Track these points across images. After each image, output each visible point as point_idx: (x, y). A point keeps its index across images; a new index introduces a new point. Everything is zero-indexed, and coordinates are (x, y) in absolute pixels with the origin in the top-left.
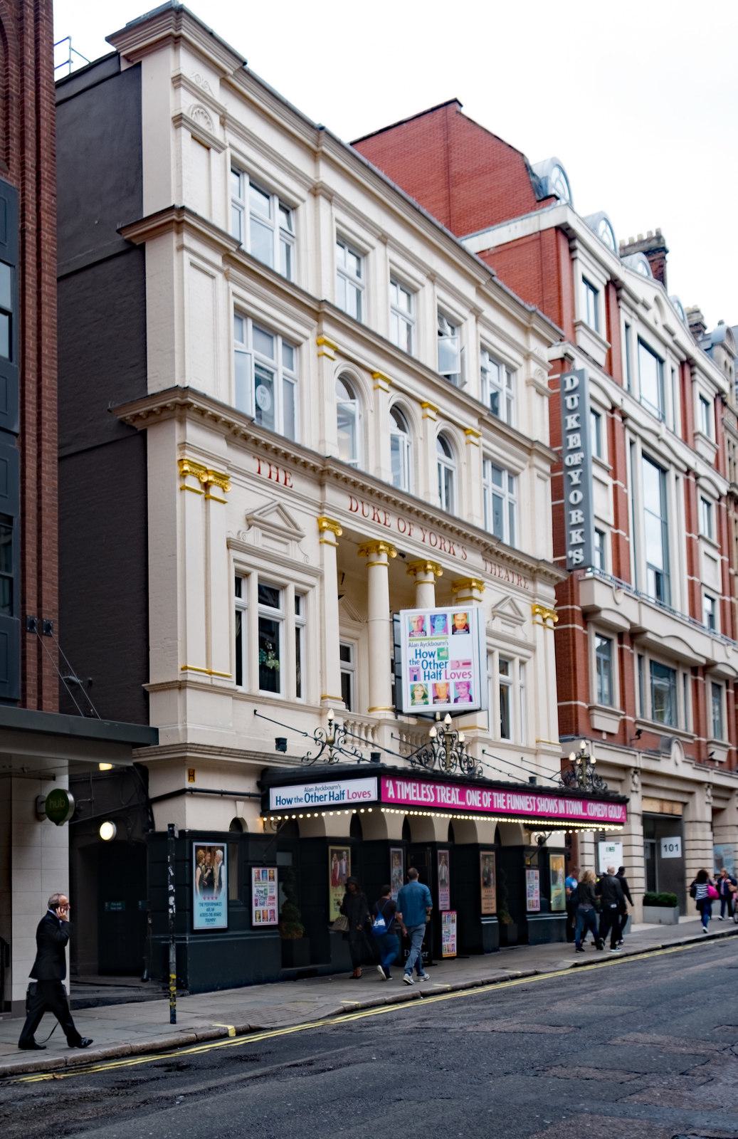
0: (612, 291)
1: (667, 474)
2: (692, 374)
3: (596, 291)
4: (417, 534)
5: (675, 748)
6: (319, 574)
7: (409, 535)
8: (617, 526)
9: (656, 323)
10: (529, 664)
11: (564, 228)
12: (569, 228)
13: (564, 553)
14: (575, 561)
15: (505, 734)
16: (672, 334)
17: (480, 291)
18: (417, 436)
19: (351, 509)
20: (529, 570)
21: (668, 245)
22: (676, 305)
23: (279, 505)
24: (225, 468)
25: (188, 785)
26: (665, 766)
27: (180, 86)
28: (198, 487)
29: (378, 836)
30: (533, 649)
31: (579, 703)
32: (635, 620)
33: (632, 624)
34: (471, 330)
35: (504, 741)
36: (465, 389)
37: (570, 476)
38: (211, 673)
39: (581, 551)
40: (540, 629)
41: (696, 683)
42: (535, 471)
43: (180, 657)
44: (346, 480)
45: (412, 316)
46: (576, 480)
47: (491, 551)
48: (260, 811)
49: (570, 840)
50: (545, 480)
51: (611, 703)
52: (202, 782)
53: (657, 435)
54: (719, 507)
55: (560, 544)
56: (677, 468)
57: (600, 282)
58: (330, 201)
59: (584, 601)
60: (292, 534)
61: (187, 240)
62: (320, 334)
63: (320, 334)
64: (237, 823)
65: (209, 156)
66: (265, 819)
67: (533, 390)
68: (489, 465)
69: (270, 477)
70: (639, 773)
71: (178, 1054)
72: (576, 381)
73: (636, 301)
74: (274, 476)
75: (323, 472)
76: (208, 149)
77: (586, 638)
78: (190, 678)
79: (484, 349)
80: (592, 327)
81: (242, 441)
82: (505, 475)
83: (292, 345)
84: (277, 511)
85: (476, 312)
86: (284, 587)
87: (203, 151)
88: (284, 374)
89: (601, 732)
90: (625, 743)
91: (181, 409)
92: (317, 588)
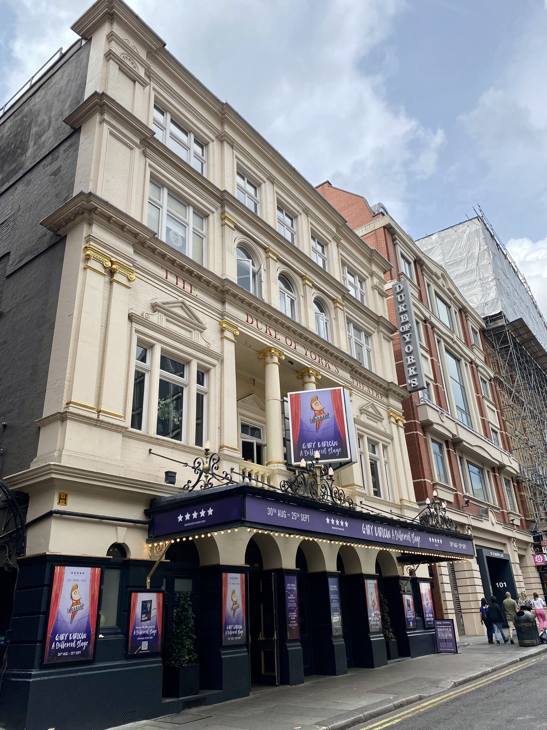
2: (466, 317)
4: (301, 350)
5: (490, 514)
7: (295, 348)
9: (444, 286)
10: (390, 448)
15: (377, 493)
16: (453, 294)
20: (386, 390)
23: (183, 303)
24: (131, 265)
25: (57, 507)
26: (485, 525)
27: (113, 39)
31: (426, 480)
33: (454, 435)
34: (333, 246)
37: (404, 337)
39: (416, 379)
40: (394, 427)
41: (495, 476)
42: (105, 126)
43: (65, 394)
44: (242, 301)
46: (408, 339)
47: (356, 372)
49: (432, 572)
50: (389, 342)
51: (447, 482)
52: (74, 505)
53: (452, 339)
54: (491, 384)
55: (400, 371)
56: (465, 359)
58: (232, 147)
59: (422, 418)
62: (223, 213)
63: (223, 213)
64: (119, 549)
65: (135, 85)
66: (150, 545)
67: (376, 292)
69: (266, 332)
71: (339, 723)
72: (411, 348)
75: (221, 291)
76: (134, 82)
79: (344, 264)
80: (409, 276)
82: (363, 334)
84: (181, 307)
86: (189, 362)
87: (131, 83)
91: (89, 214)
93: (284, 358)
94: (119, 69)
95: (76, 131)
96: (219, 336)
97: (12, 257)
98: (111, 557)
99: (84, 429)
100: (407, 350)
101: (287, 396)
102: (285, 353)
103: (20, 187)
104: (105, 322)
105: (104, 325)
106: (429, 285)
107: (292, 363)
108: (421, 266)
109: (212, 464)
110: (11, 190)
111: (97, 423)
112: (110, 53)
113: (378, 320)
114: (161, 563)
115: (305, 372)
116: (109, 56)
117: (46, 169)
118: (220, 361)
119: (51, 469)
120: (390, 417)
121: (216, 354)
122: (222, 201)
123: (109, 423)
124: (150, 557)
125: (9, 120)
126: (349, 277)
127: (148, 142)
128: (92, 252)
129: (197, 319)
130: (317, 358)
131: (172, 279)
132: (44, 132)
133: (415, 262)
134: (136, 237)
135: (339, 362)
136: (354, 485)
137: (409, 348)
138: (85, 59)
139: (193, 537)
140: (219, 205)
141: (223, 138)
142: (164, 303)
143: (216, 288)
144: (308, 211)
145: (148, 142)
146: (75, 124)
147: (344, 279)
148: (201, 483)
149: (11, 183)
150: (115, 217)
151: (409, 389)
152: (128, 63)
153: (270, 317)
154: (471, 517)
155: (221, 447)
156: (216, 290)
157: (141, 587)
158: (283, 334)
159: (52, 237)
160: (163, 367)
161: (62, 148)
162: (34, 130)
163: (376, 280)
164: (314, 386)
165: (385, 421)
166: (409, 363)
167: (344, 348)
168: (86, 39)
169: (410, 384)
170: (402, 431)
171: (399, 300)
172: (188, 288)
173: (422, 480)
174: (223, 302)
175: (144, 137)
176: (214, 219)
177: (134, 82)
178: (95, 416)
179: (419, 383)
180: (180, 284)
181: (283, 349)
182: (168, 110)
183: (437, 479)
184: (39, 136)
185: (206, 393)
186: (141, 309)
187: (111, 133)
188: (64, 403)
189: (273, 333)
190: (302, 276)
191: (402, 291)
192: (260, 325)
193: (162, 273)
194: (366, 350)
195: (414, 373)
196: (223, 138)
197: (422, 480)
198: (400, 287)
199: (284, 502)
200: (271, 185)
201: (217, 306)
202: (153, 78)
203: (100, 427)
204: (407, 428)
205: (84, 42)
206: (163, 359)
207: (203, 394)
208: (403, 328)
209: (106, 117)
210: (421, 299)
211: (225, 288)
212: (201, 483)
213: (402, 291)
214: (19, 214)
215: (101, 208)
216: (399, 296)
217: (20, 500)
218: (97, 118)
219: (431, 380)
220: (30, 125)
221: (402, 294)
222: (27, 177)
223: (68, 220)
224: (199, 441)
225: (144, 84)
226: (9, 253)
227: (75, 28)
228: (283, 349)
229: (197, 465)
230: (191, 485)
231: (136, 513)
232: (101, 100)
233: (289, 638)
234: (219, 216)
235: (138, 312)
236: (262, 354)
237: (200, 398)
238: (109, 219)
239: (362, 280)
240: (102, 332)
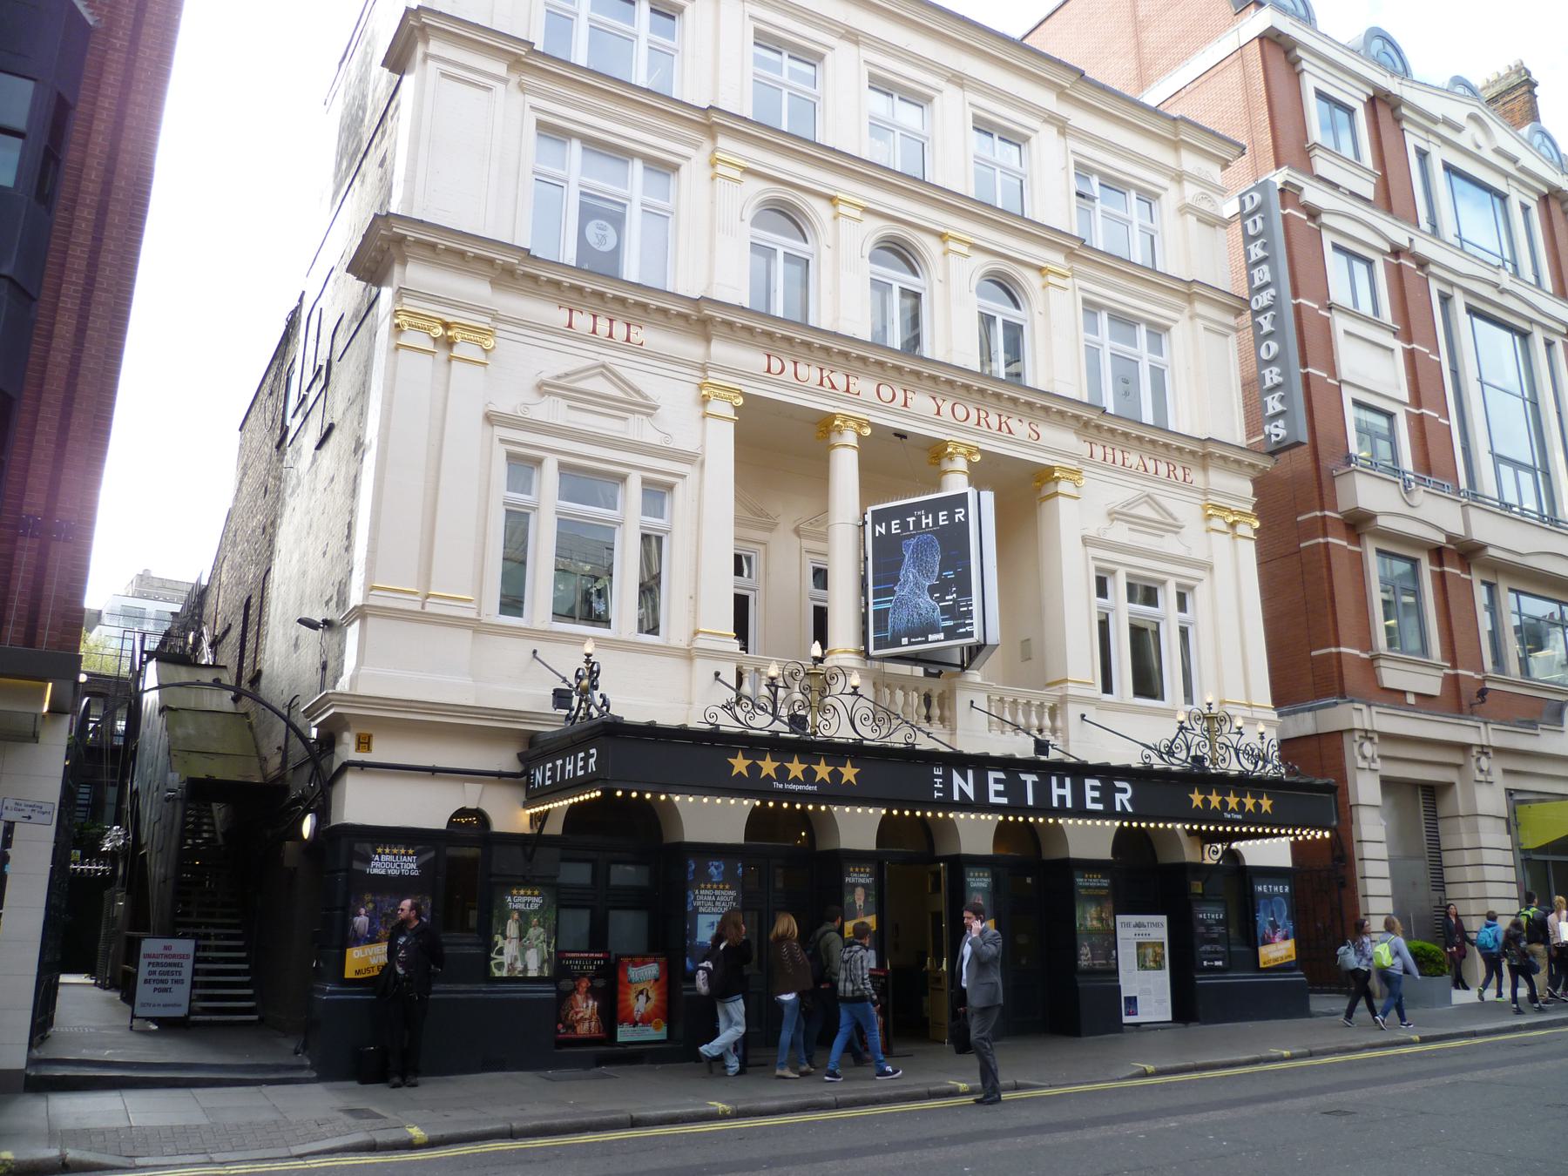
0: (1384, 114)
1: (1530, 339)
3: (1350, 111)
8: (1417, 400)
12: (1280, 34)
14: (1274, 439)
16: (1514, 160)
19: (769, 371)
21: (1535, 77)
23: (604, 366)
24: (488, 320)
28: (1224, 528)
29: (1057, 854)
30: (1208, 567)
31: (1343, 649)
32: (1458, 529)
34: (1046, 141)
35: (1107, 697)
38: (1250, 706)
39: (1281, 423)
42: (1199, 323)
45: (1022, 170)
48: (523, 798)
52: (381, 752)
53: (1496, 286)
57: (1356, 98)
59: (1344, 505)
67: (1191, 219)
68: (1103, 318)
69: (821, 384)
70: (1376, 739)
73: (1434, 120)
74: (1110, 458)
77: (1359, 561)
78: (1071, 691)
83: (663, 167)
84: (602, 374)
85: (1051, 119)
86: (1163, 583)
89: (1404, 692)
106: (1423, 155)
130: (974, 413)
131: (583, 321)
136: (1066, 680)
139: (656, 794)
142: (559, 377)
158: (871, 376)
160: (1131, 599)
164: (964, 479)
172: (620, 330)
178: (417, 607)
185: (534, 509)
186: (1096, 525)
192: (803, 370)
193: (558, 316)
197: (1333, 650)
200: (852, 48)
206: (1131, 588)
215: (412, 234)
224: (1188, 695)
231: (504, 759)
232: (418, 19)
233: (64, 978)
237: (1184, 632)
239: (1149, 197)
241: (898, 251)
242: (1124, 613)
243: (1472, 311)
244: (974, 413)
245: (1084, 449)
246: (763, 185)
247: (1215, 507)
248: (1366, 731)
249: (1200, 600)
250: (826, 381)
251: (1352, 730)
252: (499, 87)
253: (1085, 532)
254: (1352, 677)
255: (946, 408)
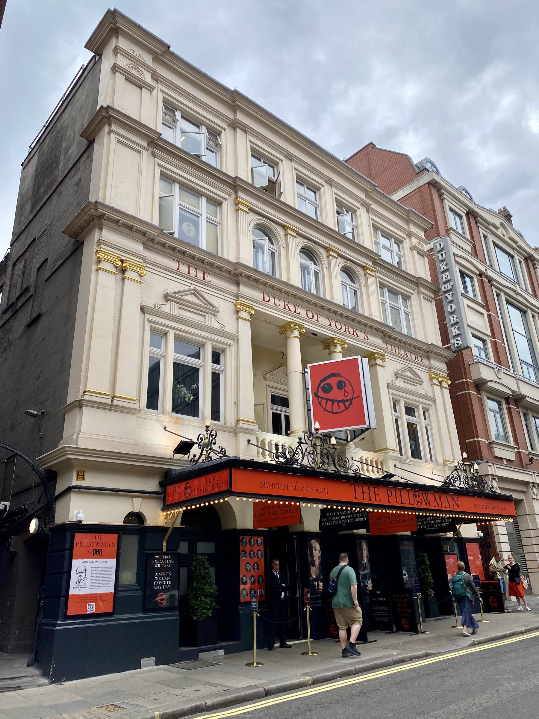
2: (534, 265)
3: (460, 217)
4: (324, 321)
6: (236, 339)
7: (317, 320)
8: (493, 336)
10: (432, 411)
11: (433, 183)
12: (436, 183)
13: (449, 342)
16: (516, 242)
17: (367, 195)
18: (324, 265)
19: (264, 300)
21: (511, 213)
22: (464, 192)
23: (195, 290)
24: (142, 261)
25: (75, 482)
28: (438, 383)
31: (480, 439)
32: (515, 389)
33: (513, 392)
34: (362, 213)
36: (282, 199)
39: (459, 339)
40: (437, 389)
46: (450, 298)
47: (390, 337)
48: (162, 506)
50: (431, 302)
51: (507, 440)
52: (90, 481)
53: (515, 291)
55: (445, 338)
56: (532, 310)
58: (245, 132)
59: (475, 376)
60: (419, 382)
61: (114, 127)
62: (237, 198)
64: (136, 517)
66: (165, 513)
67: (415, 253)
72: (454, 307)
73: (489, 223)
74: (394, 350)
75: (236, 274)
76: (141, 88)
79: (376, 228)
80: (460, 231)
81: (376, 332)
84: (194, 294)
86: (204, 345)
87: (138, 90)
88: (179, 205)
89: (502, 459)
90: (523, 467)
92: (433, 406)
93: (304, 331)
94: (125, 79)
95: (91, 143)
96: (235, 317)
97: (49, 262)
98: (127, 524)
99: (100, 414)
100: (449, 310)
101: (307, 368)
102: (305, 326)
103: (55, 198)
104: (118, 316)
105: (117, 319)
106: (485, 237)
107: (315, 335)
108: (475, 218)
109: (211, 439)
110: (49, 201)
111: (111, 407)
112: (116, 66)
113: (417, 282)
114: (175, 529)
115: (331, 342)
116: (115, 69)
117: (72, 180)
118: (236, 340)
119: (66, 451)
120: (431, 379)
121: (231, 334)
122: (235, 186)
123: (123, 407)
124: (166, 523)
125: (48, 137)
126: (383, 241)
127: (155, 143)
128: (102, 255)
129: (210, 304)
130: (343, 328)
131: (184, 269)
132: (71, 146)
133: (467, 214)
134: (145, 235)
135: (369, 329)
136: (387, 449)
137: (451, 307)
138: (98, 74)
140: (232, 191)
141: (236, 126)
142: (175, 293)
143: (229, 272)
144: (332, 182)
145: (155, 143)
146: (90, 139)
147: (377, 244)
148: (203, 457)
149: (49, 195)
150: (123, 220)
151: (453, 349)
152: (134, 72)
153: (287, 293)
154: (536, 474)
155: (238, 421)
156: (230, 274)
157: (159, 550)
158: (303, 307)
159: (74, 243)
161: (83, 159)
162: (64, 145)
163: (415, 241)
164: (341, 355)
165: (426, 384)
166: (452, 322)
167: (377, 316)
168: (98, 55)
169: (454, 344)
170: (447, 393)
171: (440, 258)
172: (200, 275)
173: (476, 439)
174: (238, 284)
175: (151, 140)
176: (228, 206)
177: (141, 88)
178: (109, 402)
179: (463, 343)
180: (193, 272)
181: (304, 322)
182: (178, 107)
183: (494, 439)
184: (67, 149)
185: (399, 417)
186: (153, 299)
187: (119, 142)
188: (81, 392)
189: (292, 308)
190: (326, 248)
191: (442, 249)
192: (277, 302)
193: (174, 265)
194: (403, 313)
195: (458, 332)
196: (236, 126)
197: (476, 439)
198: (440, 245)
199: (278, 472)
200: (289, 162)
201: (232, 288)
202: (161, 81)
203: (114, 410)
204: (453, 390)
205: (97, 58)
207: (219, 372)
208: (445, 287)
209: (114, 127)
210: (475, 253)
211: (238, 272)
212: (203, 457)
213: (442, 249)
214: (54, 223)
215: (108, 214)
216: (439, 255)
217: (51, 476)
218: (106, 129)
219: (488, 336)
220: (61, 140)
221: (443, 252)
222: (59, 188)
223: (83, 229)
225: (151, 89)
226: (47, 259)
227: (88, 46)
228: (304, 322)
229: (200, 441)
230: (196, 458)
232: (107, 113)
234: (233, 202)
235: (150, 303)
236: (284, 329)
237: (216, 378)
238: (117, 222)
239: (399, 242)
240: (117, 325)
241: (307, 252)
242: (170, 357)
243: (508, 302)
244: (343, 328)
245: (385, 346)
246: (257, 217)
247: (435, 374)
248: (493, 475)
249: (228, 359)
250: (286, 306)
251: (489, 475)
252: (145, 153)
253: (388, 382)
254: (485, 451)
255: (333, 324)
